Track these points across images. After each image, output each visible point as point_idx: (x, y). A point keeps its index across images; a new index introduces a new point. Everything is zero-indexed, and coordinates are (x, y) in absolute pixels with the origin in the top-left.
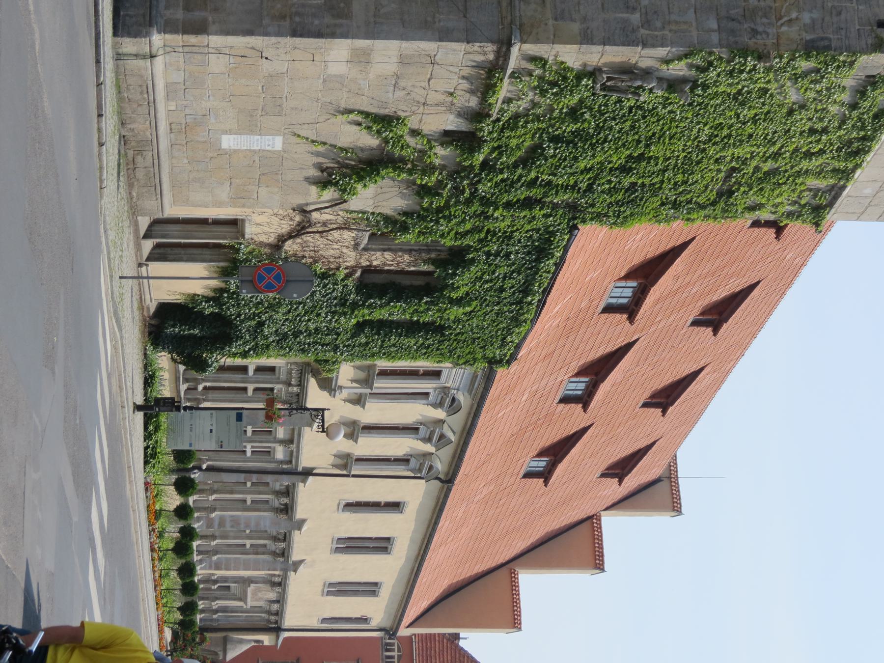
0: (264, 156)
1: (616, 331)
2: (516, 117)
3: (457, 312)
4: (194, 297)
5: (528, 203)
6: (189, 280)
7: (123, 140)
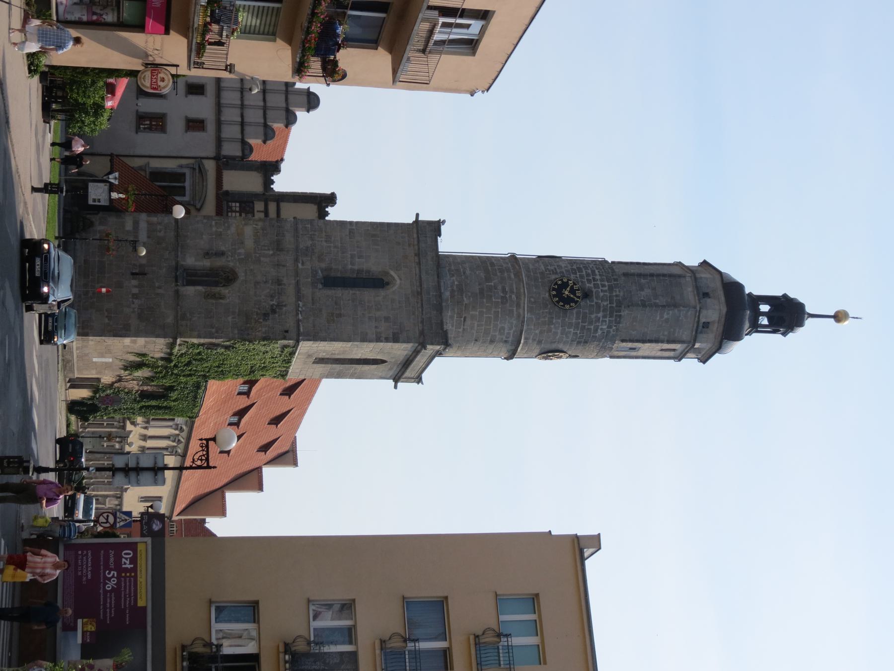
0: (106, 363)
1: (243, 402)
2: (182, 354)
3: (173, 404)
4: (84, 398)
5: (190, 375)
6: (83, 393)
7: (63, 360)
